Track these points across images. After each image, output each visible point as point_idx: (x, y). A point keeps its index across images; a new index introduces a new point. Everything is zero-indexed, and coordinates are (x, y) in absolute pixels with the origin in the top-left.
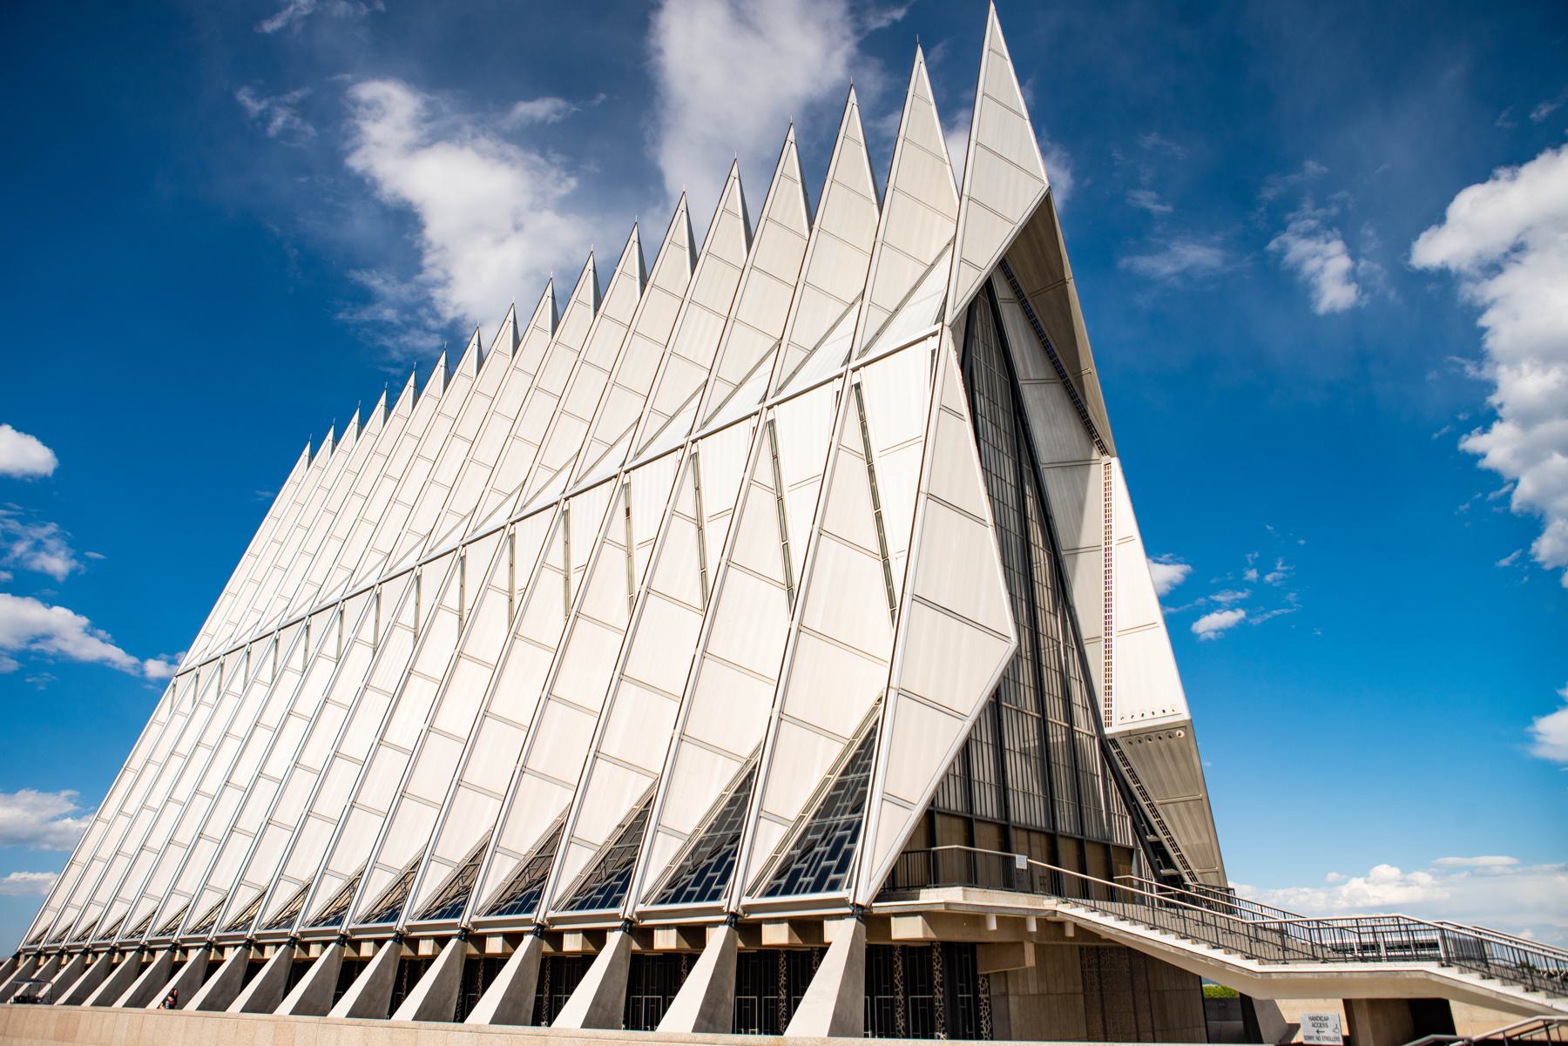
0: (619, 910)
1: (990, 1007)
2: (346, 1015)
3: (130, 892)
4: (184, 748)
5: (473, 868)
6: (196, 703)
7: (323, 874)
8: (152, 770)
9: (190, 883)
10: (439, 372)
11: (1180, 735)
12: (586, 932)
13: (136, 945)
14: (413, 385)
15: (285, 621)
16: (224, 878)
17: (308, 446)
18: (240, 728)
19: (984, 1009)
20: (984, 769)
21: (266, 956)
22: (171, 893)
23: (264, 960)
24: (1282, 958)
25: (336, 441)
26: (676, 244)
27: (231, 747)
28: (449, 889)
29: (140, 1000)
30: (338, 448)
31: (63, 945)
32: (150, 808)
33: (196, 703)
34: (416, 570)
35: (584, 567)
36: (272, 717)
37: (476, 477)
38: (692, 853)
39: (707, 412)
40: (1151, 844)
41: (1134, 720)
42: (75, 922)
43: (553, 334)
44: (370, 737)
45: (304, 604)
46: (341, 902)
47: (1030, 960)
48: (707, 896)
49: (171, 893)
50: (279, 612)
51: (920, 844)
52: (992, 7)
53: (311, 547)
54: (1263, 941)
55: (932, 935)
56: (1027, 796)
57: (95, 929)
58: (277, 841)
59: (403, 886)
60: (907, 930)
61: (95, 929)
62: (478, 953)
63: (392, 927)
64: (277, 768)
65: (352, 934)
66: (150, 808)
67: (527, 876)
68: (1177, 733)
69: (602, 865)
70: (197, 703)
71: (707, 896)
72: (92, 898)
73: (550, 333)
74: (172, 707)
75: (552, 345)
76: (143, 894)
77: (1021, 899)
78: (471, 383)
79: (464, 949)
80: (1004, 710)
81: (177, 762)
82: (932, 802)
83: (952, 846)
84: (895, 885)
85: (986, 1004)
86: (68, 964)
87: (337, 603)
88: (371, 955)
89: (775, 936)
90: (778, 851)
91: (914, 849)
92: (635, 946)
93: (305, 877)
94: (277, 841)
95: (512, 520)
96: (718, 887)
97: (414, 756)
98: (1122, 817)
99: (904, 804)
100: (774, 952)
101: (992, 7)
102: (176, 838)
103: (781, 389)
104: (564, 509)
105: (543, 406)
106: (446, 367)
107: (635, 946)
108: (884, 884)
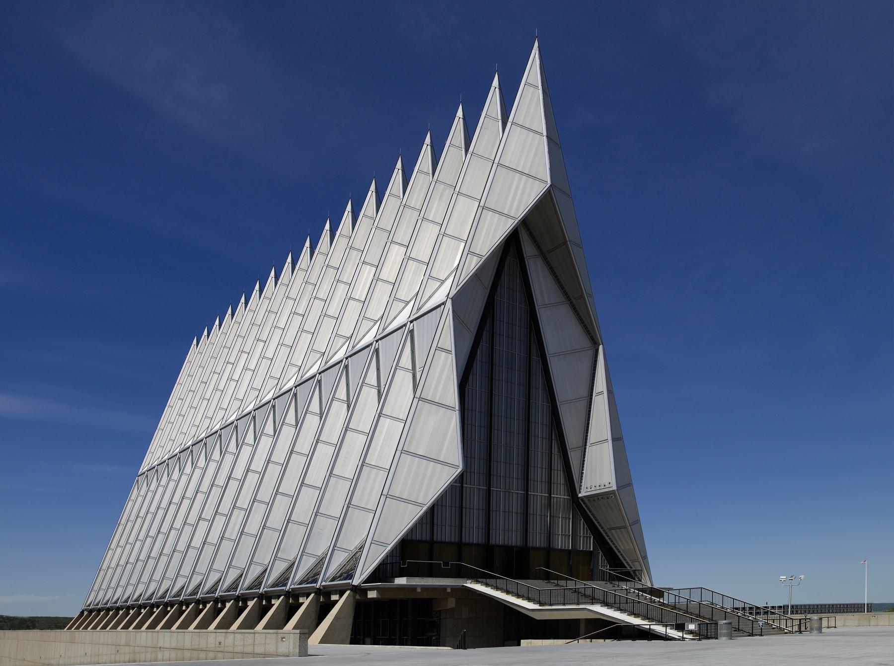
4: (176, 499)
6: (208, 460)
7: (333, 550)
8: (130, 524)
9: (202, 568)
10: (397, 177)
14: (244, 302)
15: (258, 404)
16: (241, 561)
17: (461, 106)
18: (221, 481)
22: (229, 568)
25: (277, 278)
26: (367, 216)
27: (216, 491)
29: (126, 627)
30: (316, 251)
31: (152, 601)
32: (205, 520)
33: (208, 460)
34: (252, 412)
36: (238, 473)
37: (382, 292)
39: (283, 382)
42: (171, 587)
43: (433, 174)
44: (323, 473)
45: (269, 392)
49: (229, 568)
50: (236, 409)
53: (289, 341)
55: (380, 597)
57: (169, 593)
58: (247, 543)
61: (169, 593)
63: (350, 583)
64: (244, 502)
66: (205, 520)
70: (208, 460)
72: (194, 571)
73: (431, 175)
74: (192, 464)
75: (433, 183)
76: (164, 577)
78: (400, 201)
79: (354, 597)
81: (139, 520)
84: (375, 576)
86: (157, 611)
87: (270, 401)
88: (338, 599)
92: (358, 597)
93: (320, 552)
95: (376, 339)
97: (323, 490)
98: (566, 536)
102: (192, 545)
103: (420, 308)
104: (410, 329)
105: (429, 233)
106: (377, 192)
107: (358, 597)
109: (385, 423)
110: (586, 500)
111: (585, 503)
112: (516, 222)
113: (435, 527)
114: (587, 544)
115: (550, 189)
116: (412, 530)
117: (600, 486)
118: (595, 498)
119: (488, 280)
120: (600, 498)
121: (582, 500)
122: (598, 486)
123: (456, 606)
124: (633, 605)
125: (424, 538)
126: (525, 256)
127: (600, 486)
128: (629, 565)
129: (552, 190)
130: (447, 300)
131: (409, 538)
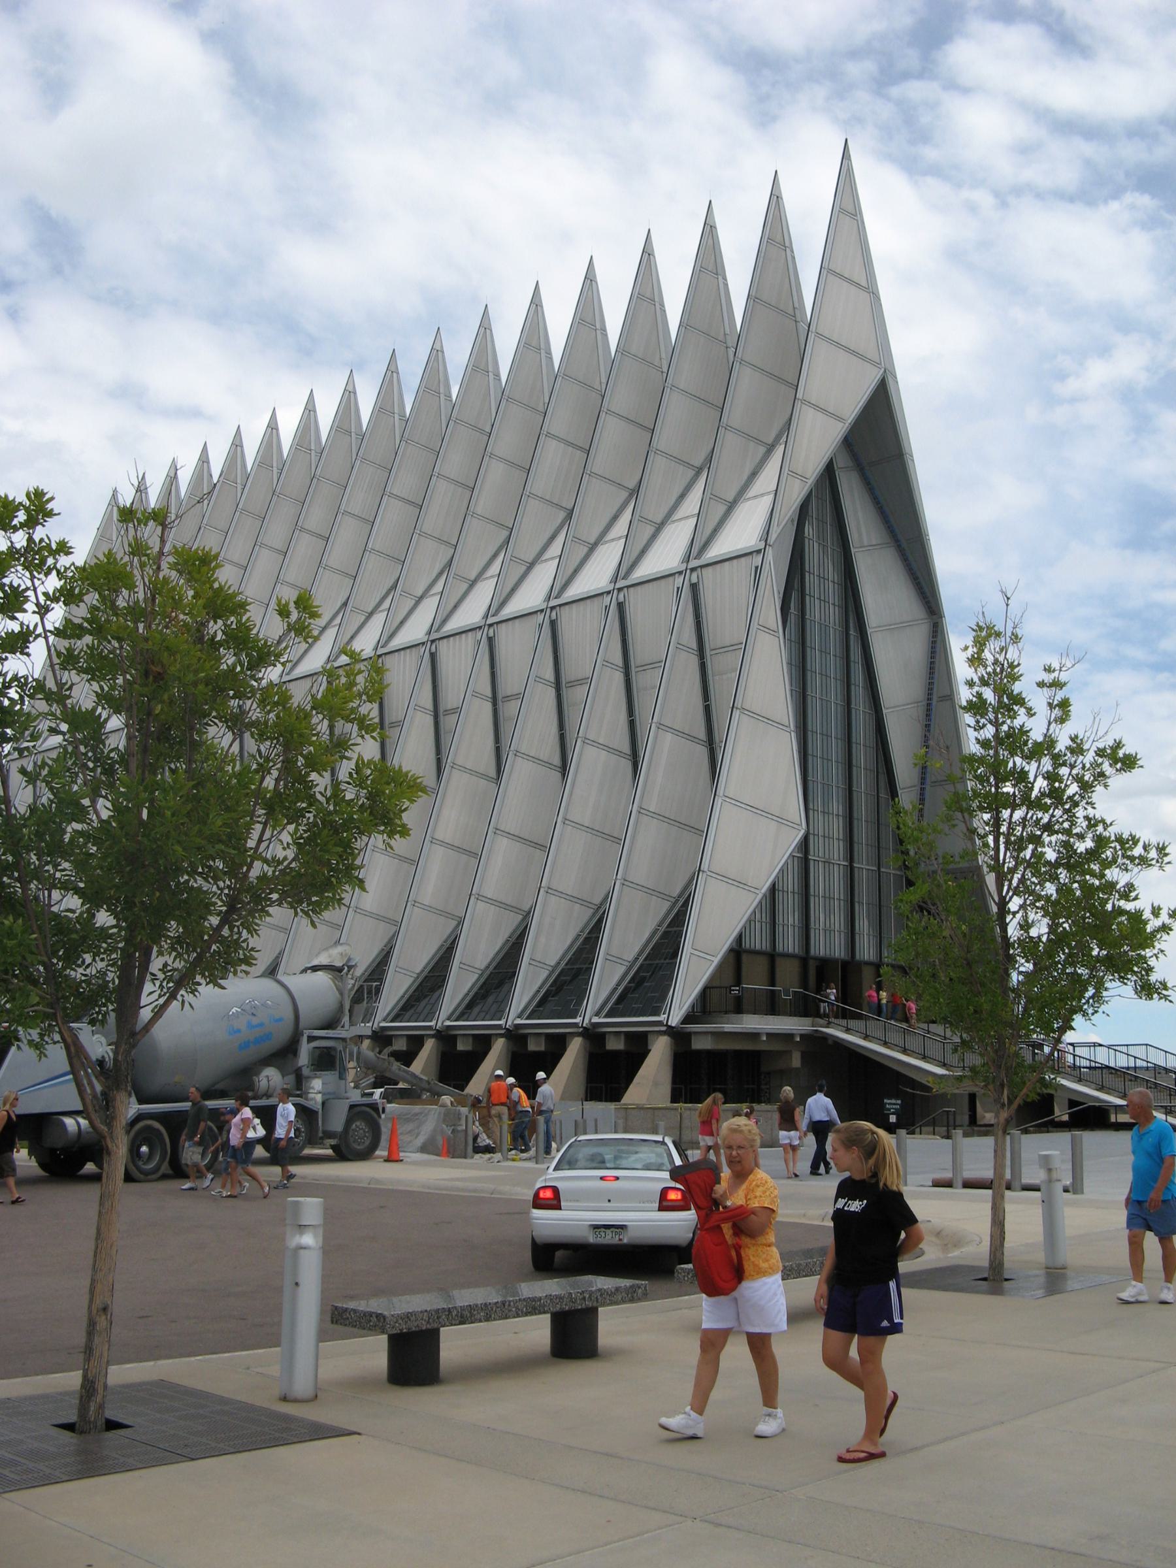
0: (578, 1020)
12: (409, 1037)
20: (790, 918)
38: (555, 981)
47: (796, 1061)
51: (728, 979)
56: (828, 932)
80: (812, 863)
82: (740, 938)
83: (755, 984)
84: (703, 1008)
89: (615, 1045)
90: (618, 984)
91: (714, 985)
99: (803, 478)
100: (616, 1054)
108: (693, 1006)
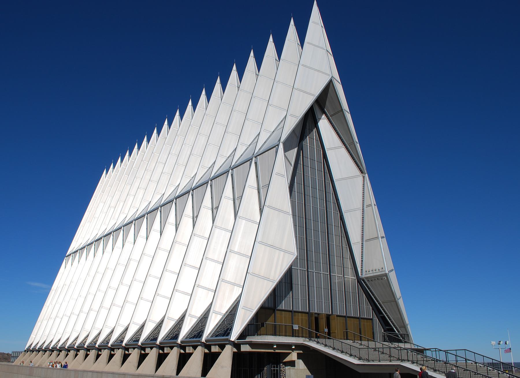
1: (285, 373)
2: (201, 376)
3: (54, 331)
5: (182, 321)
11: (385, 278)
13: (83, 348)
19: (282, 373)
21: (130, 352)
23: (130, 354)
24: (390, 359)
28: (174, 329)
35: (268, 185)
40: (381, 317)
41: (370, 273)
46: (139, 333)
48: (226, 335)
52: (315, 2)
54: (386, 354)
59: (178, 326)
60: (245, 348)
62: (237, 351)
65: (99, 347)
67: (226, 322)
68: (384, 278)
69: (225, 320)
71: (226, 335)
77: (292, 339)
84: (242, 336)
85: (283, 372)
94: (116, 311)
96: (229, 332)
101: (315, 2)
109: (195, 239)
110: (366, 281)
111: (365, 283)
112: (315, 97)
113: (276, 297)
114: (368, 312)
115: (332, 79)
116: (264, 302)
117: (375, 270)
118: (373, 279)
119: (299, 134)
120: (376, 278)
121: (363, 280)
122: (371, 270)
123: (242, 351)
124: (379, 359)
125: (270, 306)
126: (317, 119)
127: (375, 270)
128: (397, 330)
129: (332, 79)
130: (279, 144)
131: (264, 306)
